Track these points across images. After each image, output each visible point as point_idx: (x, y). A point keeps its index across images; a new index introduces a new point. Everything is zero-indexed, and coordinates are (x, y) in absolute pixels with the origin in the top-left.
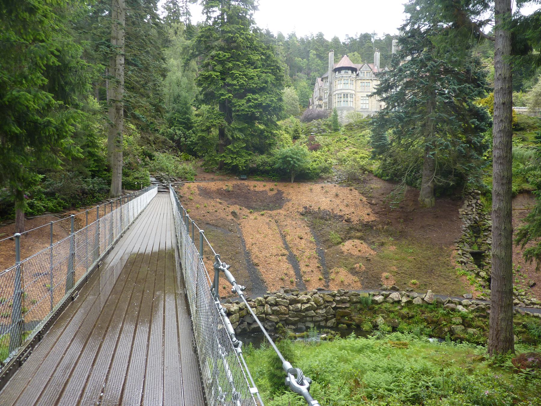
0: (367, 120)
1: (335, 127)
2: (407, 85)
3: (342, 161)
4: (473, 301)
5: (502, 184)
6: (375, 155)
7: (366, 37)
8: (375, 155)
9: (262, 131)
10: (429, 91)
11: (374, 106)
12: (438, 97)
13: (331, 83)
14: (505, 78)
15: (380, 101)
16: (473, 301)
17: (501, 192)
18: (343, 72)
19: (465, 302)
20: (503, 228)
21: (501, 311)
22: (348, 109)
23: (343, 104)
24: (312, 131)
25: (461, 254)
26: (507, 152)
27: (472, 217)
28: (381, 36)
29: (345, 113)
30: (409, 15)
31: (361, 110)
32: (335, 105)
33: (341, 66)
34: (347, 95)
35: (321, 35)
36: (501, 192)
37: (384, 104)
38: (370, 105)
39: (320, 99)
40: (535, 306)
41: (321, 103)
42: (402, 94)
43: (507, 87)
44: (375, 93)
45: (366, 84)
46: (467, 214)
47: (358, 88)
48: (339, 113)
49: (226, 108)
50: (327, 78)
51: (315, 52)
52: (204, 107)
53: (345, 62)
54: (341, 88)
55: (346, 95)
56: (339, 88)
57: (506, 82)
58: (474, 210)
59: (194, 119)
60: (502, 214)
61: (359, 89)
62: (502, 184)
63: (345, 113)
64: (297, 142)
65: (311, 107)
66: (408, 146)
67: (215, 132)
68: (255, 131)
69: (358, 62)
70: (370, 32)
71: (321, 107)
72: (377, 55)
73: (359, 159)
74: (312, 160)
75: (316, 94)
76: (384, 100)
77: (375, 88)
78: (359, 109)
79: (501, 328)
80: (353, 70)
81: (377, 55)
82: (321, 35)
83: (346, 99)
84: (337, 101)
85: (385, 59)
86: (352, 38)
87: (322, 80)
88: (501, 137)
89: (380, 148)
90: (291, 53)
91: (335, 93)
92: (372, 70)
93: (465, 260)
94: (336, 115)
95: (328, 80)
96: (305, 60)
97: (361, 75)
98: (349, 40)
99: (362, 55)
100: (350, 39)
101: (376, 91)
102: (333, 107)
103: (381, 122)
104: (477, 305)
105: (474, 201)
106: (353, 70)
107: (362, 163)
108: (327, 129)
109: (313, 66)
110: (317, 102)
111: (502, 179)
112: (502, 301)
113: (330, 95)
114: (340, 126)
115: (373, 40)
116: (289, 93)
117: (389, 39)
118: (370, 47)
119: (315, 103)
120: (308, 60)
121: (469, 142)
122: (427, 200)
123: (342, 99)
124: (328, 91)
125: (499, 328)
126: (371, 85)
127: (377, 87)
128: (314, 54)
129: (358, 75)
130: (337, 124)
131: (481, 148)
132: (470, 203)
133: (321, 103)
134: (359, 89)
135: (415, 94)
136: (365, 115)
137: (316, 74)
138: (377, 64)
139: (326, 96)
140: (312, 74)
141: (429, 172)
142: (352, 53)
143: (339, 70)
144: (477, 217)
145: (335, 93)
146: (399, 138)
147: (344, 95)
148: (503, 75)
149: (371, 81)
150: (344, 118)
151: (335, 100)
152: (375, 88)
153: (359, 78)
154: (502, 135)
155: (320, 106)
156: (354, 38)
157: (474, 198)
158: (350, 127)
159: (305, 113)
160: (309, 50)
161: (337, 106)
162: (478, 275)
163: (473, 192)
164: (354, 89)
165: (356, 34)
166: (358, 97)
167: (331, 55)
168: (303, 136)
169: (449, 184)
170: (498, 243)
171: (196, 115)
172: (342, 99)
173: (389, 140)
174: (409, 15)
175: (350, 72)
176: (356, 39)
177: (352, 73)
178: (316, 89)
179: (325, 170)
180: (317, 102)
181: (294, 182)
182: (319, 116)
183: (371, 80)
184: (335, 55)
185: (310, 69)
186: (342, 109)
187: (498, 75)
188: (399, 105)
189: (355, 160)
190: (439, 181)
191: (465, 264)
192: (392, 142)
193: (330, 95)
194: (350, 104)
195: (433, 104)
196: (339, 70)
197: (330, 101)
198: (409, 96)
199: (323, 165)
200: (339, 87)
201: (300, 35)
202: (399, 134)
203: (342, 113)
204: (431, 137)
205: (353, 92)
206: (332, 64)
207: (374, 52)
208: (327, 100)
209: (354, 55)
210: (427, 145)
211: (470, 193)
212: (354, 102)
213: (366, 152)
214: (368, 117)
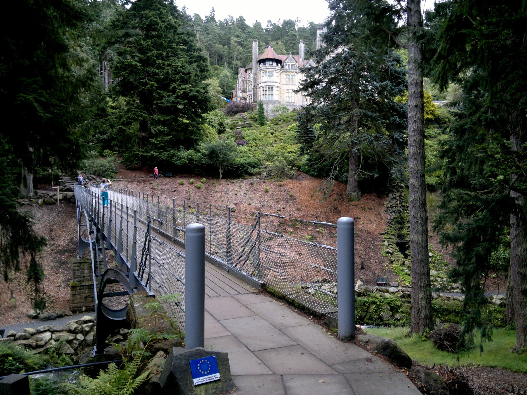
0: (293, 114)
1: (261, 120)
2: (332, 82)
3: (270, 157)
4: (400, 288)
5: (417, 177)
6: (303, 151)
7: (289, 24)
8: (303, 151)
9: (187, 125)
10: (352, 87)
11: (302, 101)
12: (361, 94)
13: (255, 75)
14: (417, 83)
15: (306, 96)
16: (400, 288)
17: (416, 184)
18: (267, 64)
19: (392, 289)
20: (419, 216)
21: (421, 291)
22: (274, 102)
23: (268, 98)
24: (237, 124)
25: (387, 245)
26: (420, 149)
27: (396, 210)
28: (303, 24)
29: (271, 107)
30: (333, 12)
31: (287, 104)
32: (260, 97)
33: (264, 58)
34: (272, 88)
35: (241, 20)
36: (416, 184)
37: (309, 100)
38: (296, 98)
39: (244, 91)
40: (455, 291)
41: (245, 95)
42: (327, 89)
43: (419, 91)
44: (301, 90)
45: (291, 77)
46: (392, 207)
47: (283, 80)
48: (264, 106)
49: (148, 100)
50: (251, 69)
51: (236, 39)
52: (122, 100)
53: (269, 53)
54: (266, 81)
55: (271, 88)
56: (264, 81)
57: (418, 87)
58: (398, 202)
59: (109, 110)
60: (418, 204)
61: (284, 82)
62: (417, 177)
63: (271, 107)
64: (223, 136)
65: (234, 99)
66: (334, 139)
67: (135, 126)
68: (179, 126)
69: (283, 54)
70: (293, 19)
71: (246, 100)
72: (302, 47)
73: (287, 154)
74: (241, 155)
75: (239, 85)
76: (309, 95)
77: (301, 84)
78: (284, 103)
79: (421, 306)
80: (278, 62)
81: (302, 47)
82: (241, 20)
83: (271, 92)
84: (262, 93)
85: (309, 54)
86: (275, 24)
87: (246, 71)
88: (415, 135)
89: (306, 137)
90: (210, 40)
91: (260, 86)
92: (297, 62)
93: (391, 250)
94: (261, 109)
95: (253, 71)
96: (226, 47)
97: (286, 67)
98: (272, 27)
99: (285, 43)
100: (272, 25)
101: (301, 87)
102: (258, 101)
103: (306, 117)
104: (403, 292)
105: (398, 194)
106: (278, 62)
107: (290, 159)
108: (253, 123)
109: (235, 54)
110: (240, 95)
111: (417, 173)
112: (421, 282)
113: (255, 87)
114: (267, 120)
115: (296, 28)
116: (213, 84)
117: (313, 29)
118: (294, 35)
119: (239, 96)
120: (229, 47)
121: (392, 137)
122: (353, 194)
123: (268, 92)
124: (252, 84)
125: (420, 307)
126: (296, 77)
127: (303, 83)
128: (236, 42)
129: (282, 67)
130: (263, 118)
131: (404, 144)
132: (394, 196)
133: (245, 95)
134: (284, 82)
135: (340, 91)
136: (291, 109)
137: (239, 63)
138: (302, 56)
139: (251, 88)
140: (234, 62)
141: (354, 166)
142: (276, 42)
143: (263, 61)
144: (401, 210)
145: (260, 86)
146: (325, 133)
147: (269, 88)
148: (415, 81)
149: (296, 74)
150: (269, 111)
151: (260, 93)
152: (301, 84)
153: (284, 70)
154: (416, 134)
155: (244, 98)
156: (277, 24)
157: (398, 191)
158: (276, 122)
159: (229, 105)
160: (230, 36)
161: (262, 99)
162: (403, 264)
163: (397, 185)
164: (279, 82)
165: (279, 20)
166: (281, 89)
167: (255, 45)
168: (228, 130)
169: (373, 177)
170: (415, 230)
171: (112, 107)
172: (268, 92)
173: (316, 133)
174: (333, 12)
175: (275, 64)
176: (279, 26)
177: (277, 65)
178: (240, 80)
179: (255, 165)
180: (240, 95)
181: (223, 178)
182: (244, 109)
183: (297, 73)
184: (260, 46)
185: (231, 58)
186: (268, 102)
187: (411, 80)
188: (324, 100)
189: (283, 155)
190: (364, 175)
191: (391, 254)
192: (318, 138)
193: (255, 87)
194: (275, 98)
195: (357, 100)
196: (263, 61)
197: (255, 93)
198: (335, 90)
199: (252, 160)
200: (264, 79)
201: (219, 18)
202: (326, 128)
203: (267, 106)
204: (355, 133)
205: (278, 85)
206: (255, 56)
207: (299, 43)
208: (251, 93)
209: (277, 43)
210: (352, 141)
211: (394, 186)
212: (280, 95)
213: (295, 147)
214: (294, 110)
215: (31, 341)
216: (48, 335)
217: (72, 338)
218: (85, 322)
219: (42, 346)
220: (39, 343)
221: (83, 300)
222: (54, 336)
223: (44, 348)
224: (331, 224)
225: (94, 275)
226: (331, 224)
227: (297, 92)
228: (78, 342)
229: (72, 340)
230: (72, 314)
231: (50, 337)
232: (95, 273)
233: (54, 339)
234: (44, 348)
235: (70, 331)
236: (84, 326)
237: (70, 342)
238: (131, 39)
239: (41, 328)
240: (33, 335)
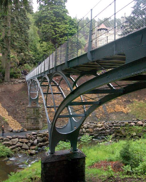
106: (106, 30)
215: (10, 142)
216: (17, 139)
217: (28, 141)
218: (33, 135)
219: (15, 145)
220: (13, 143)
221: (31, 125)
222: (20, 140)
223: (16, 146)
224: (111, 69)
225: (45, 107)
226: (111, 69)
227: (132, 7)
228: (30, 144)
229: (28, 142)
230: (27, 131)
231: (18, 140)
232: (46, 105)
233: (20, 142)
234: (16, 146)
235: (27, 139)
236: (33, 136)
237: (26, 143)
238: (15, 19)
239: (14, 136)
240: (10, 139)
